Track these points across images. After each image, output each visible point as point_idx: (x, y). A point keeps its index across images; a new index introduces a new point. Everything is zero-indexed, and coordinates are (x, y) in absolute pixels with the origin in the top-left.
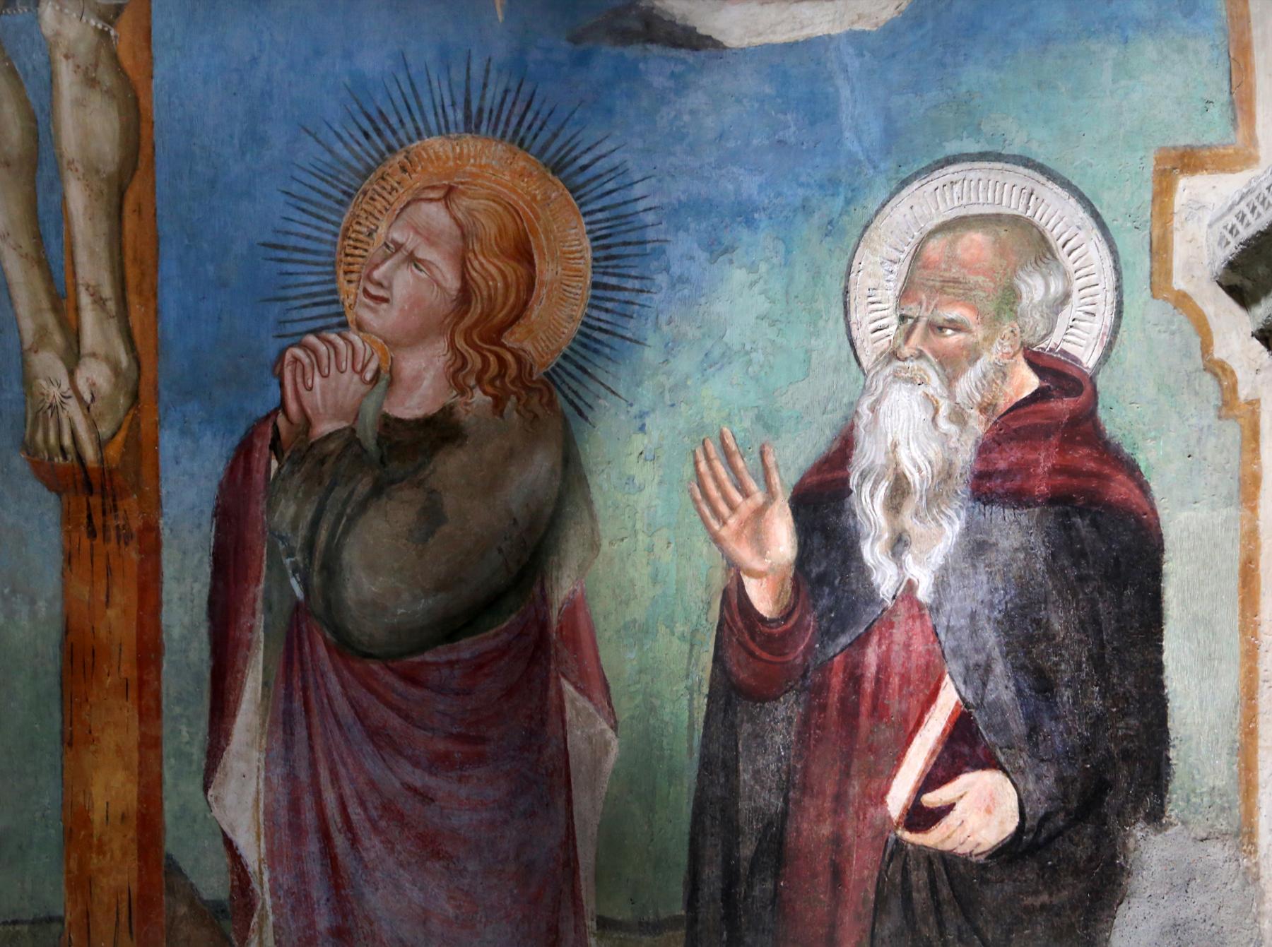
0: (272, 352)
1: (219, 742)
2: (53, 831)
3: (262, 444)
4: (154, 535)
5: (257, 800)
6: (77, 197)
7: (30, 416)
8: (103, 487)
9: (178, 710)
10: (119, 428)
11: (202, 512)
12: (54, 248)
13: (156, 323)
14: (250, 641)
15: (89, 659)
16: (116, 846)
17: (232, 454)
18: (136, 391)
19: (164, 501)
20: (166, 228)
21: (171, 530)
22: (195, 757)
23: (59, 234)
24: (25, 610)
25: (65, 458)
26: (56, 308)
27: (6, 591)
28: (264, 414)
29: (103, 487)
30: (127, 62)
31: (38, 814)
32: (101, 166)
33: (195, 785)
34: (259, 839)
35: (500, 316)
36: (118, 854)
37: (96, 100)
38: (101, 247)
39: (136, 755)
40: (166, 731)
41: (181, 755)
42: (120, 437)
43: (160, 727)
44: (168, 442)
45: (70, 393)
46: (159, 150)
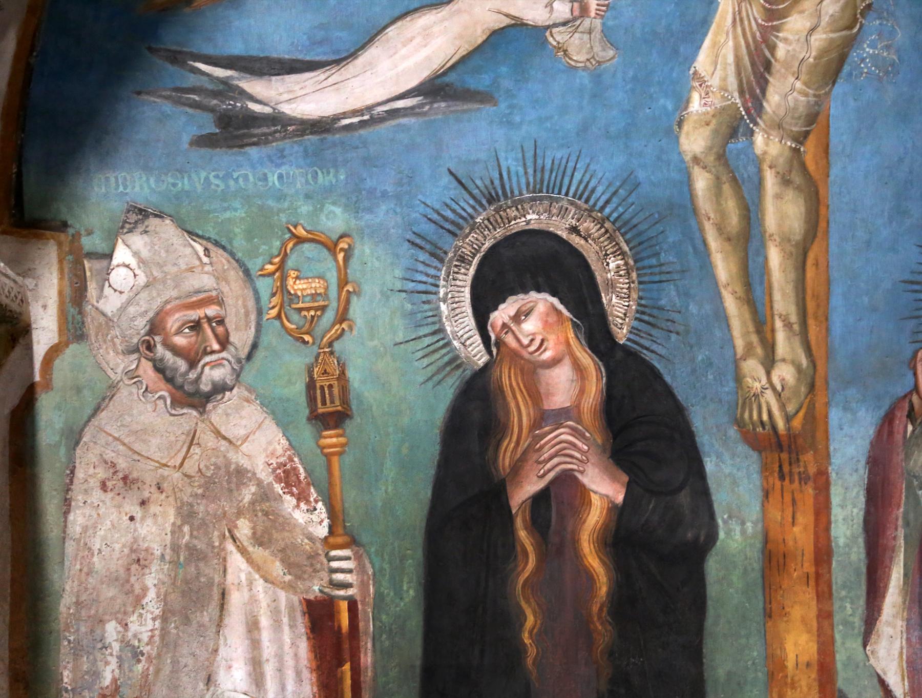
0: (908, 354)
1: (873, 615)
2: (760, 674)
3: (901, 415)
4: (825, 477)
5: (901, 653)
6: (775, 257)
7: (740, 402)
8: (790, 447)
9: (843, 593)
10: (800, 408)
11: (858, 461)
12: (758, 291)
13: (827, 336)
14: (894, 546)
15: (781, 561)
16: (804, 683)
17: (880, 422)
18: (811, 382)
19: (832, 454)
20: (835, 274)
21: (837, 474)
22: (857, 625)
23: (762, 283)
24: (738, 529)
25: (764, 428)
26: (759, 331)
27: (725, 516)
28: (903, 394)
29: (790, 447)
30: (811, 167)
31: (750, 663)
32: (792, 237)
33: (857, 644)
34: (903, 680)
35: (369, 660)
36: (805, 689)
37: (790, 194)
38: (790, 289)
39: (815, 624)
40: (836, 606)
41: (846, 623)
42: (801, 414)
43: (832, 604)
44: (835, 415)
45: (767, 386)
46: (832, 225)
